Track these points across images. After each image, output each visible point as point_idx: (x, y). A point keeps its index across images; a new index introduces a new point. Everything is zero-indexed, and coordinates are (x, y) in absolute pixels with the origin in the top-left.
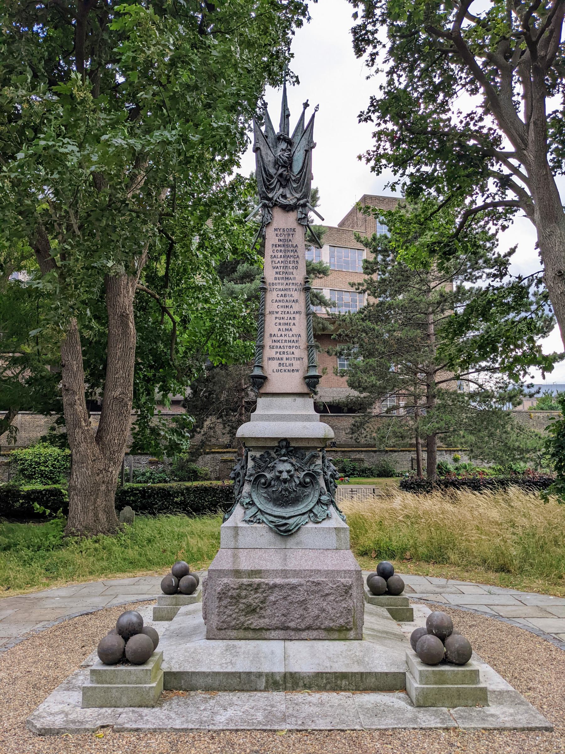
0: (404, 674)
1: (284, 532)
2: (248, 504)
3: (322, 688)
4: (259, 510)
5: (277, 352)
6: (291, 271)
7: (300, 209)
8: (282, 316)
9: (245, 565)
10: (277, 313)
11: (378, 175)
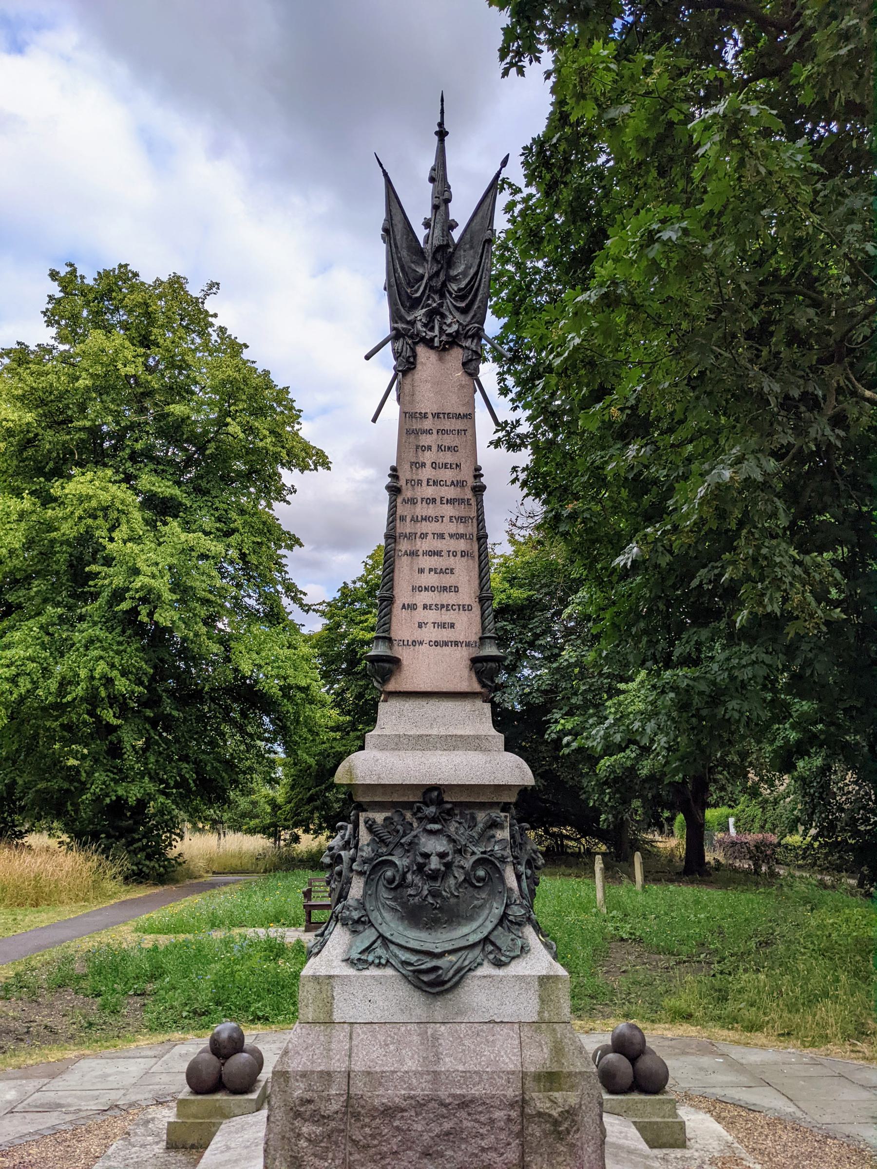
4: (381, 936)
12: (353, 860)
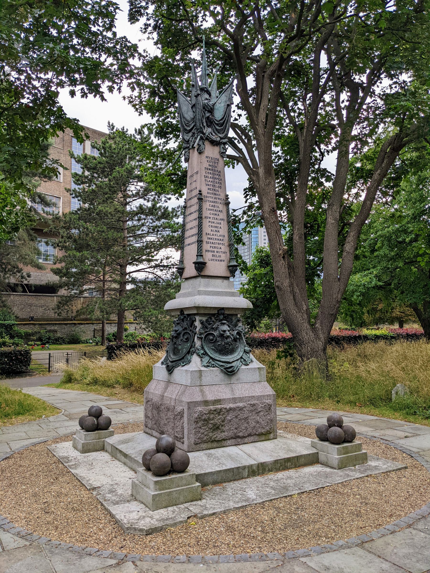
1: (230, 372)
2: (203, 354)
3: (278, 470)
4: (211, 358)
5: (211, 247)
6: (217, 189)
7: (222, 146)
8: (213, 221)
9: (210, 397)
10: (210, 218)
11: (139, 115)
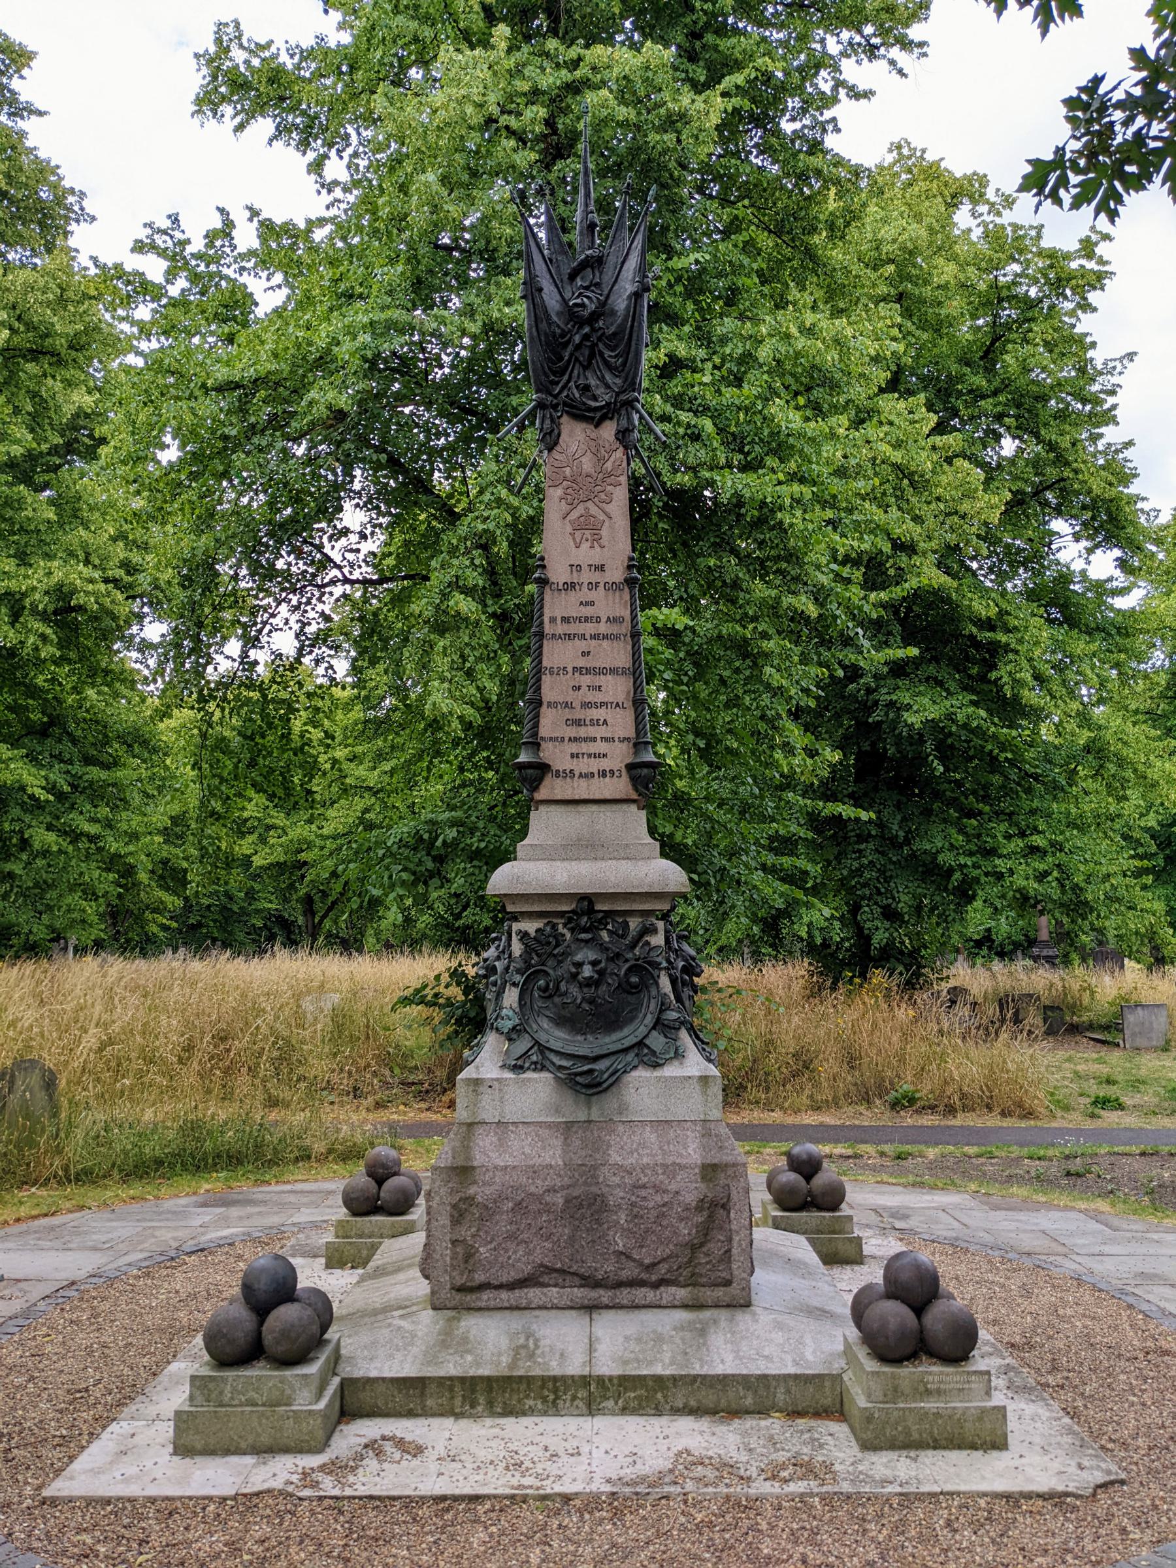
0: (837, 1378)
12: (507, 969)
